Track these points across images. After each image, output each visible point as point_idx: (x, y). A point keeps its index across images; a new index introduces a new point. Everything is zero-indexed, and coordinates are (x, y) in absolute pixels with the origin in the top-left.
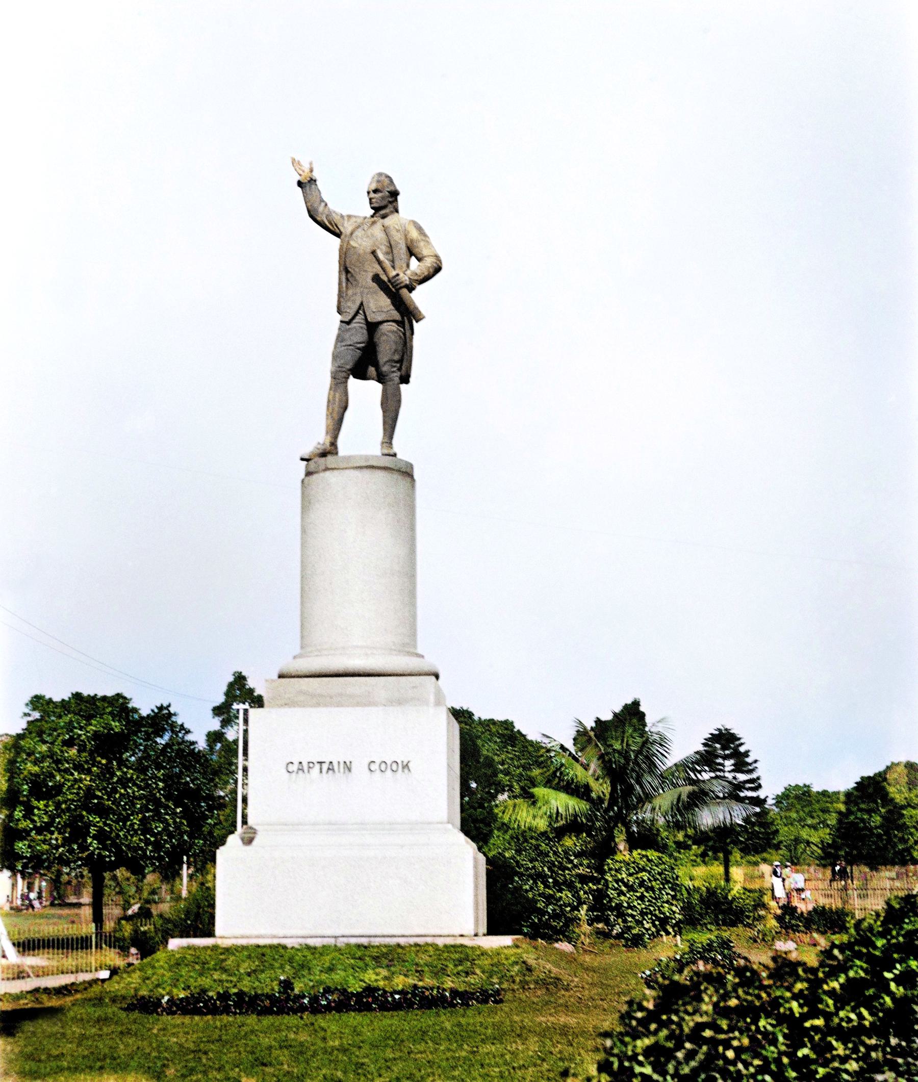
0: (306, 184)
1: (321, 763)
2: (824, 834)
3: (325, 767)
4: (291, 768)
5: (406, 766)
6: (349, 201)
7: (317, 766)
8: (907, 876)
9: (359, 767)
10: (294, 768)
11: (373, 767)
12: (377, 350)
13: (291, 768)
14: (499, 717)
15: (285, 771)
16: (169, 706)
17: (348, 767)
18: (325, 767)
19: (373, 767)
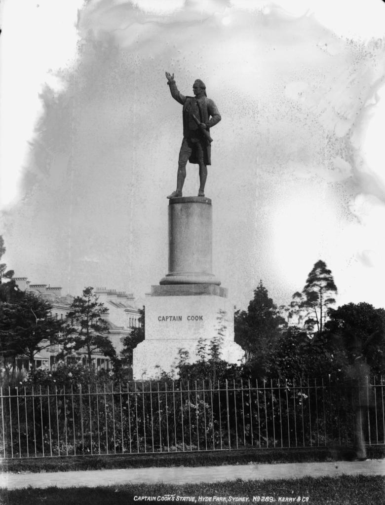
0: (171, 84)
1: (171, 317)
2: (29, 464)
3: (172, 318)
4: (160, 319)
5: (201, 318)
6: (187, 91)
7: (169, 318)
8: (274, 455)
9: (184, 319)
10: (161, 319)
11: (189, 318)
12: (196, 146)
13: (160, 319)
14: (370, 303)
15: (187, 319)
16: (106, 288)
17: (180, 318)
18: (172, 318)
19: (189, 318)
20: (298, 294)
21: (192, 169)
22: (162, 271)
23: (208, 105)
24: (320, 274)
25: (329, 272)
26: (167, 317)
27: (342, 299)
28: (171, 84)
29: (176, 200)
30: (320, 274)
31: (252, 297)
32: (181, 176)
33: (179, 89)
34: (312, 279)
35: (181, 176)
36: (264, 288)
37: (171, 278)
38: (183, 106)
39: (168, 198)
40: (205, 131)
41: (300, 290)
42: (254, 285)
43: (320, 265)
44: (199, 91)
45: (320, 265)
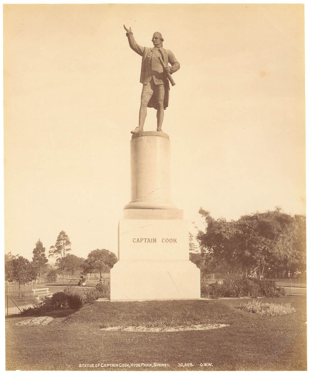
1: (146, 239)
3: (147, 240)
5: (175, 241)
6: (146, 43)
7: (144, 240)
9: (159, 241)
10: (136, 240)
11: (164, 241)
17: (155, 240)
18: (147, 240)
20: (52, 247)
21: (152, 112)
22: (128, 199)
23: (168, 54)
24: (63, 237)
25: (67, 236)
26: (142, 239)
27: (71, 253)
28: (129, 34)
29: (136, 136)
30: (63, 237)
31: (35, 247)
32: (142, 117)
33: (136, 39)
34: (59, 240)
35: (142, 117)
36: (41, 242)
37: (135, 204)
38: (142, 57)
39: (132, 133)
40: (169, 74)
41: (54, 245)
42: (36, 242)
43: (62, 233)
44: (158, 41)
45: (62, 233)
